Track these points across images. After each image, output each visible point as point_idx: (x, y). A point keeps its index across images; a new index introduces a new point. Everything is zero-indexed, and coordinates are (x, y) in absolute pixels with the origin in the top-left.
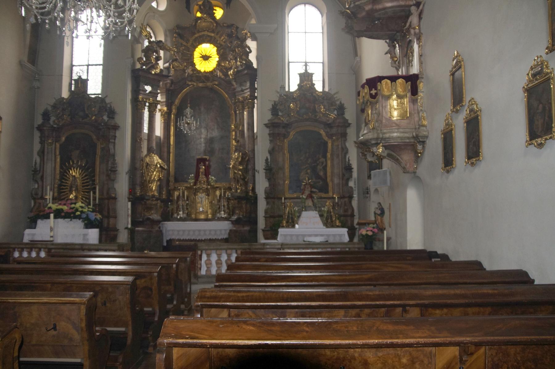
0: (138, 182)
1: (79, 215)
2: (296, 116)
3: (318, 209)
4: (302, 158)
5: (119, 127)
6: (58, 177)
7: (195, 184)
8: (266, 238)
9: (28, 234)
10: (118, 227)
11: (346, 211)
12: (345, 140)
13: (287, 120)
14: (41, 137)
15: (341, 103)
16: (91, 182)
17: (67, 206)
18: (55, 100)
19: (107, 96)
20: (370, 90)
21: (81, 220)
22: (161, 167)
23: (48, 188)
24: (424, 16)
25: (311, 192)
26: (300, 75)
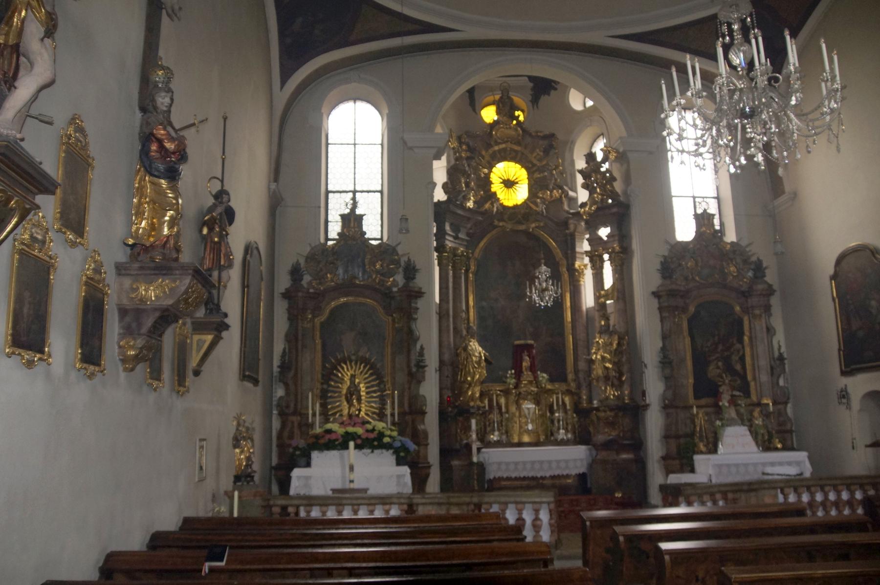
7: (517, 386)
9: (299, 478)
12: (770, 315)
14: (289, 310)
15: (758, 259)
18: (309, 249)
19: (399, 244)
21: (391, 451)
26: (343, 216)
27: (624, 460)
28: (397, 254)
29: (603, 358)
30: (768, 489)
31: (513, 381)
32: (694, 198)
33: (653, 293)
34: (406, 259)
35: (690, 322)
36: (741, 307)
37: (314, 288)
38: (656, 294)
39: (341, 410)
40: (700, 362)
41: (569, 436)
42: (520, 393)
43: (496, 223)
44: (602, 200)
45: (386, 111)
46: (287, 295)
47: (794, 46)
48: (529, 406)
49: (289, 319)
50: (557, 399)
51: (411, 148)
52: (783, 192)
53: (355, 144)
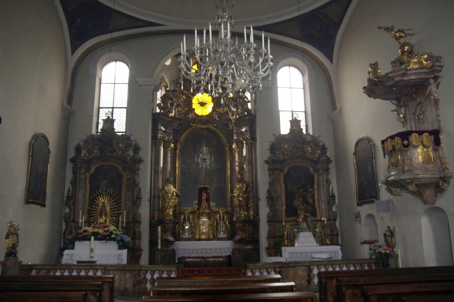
0: (156, 208)
1: (114, 238)
2: (289, 154)
3: (311, 230)
4: (295, 188)
5: (143, 160)
6: (87, 202)
7: (198, 209)
8: (270, 255)
9: (67, 255)
10: (142, 248)
11: (332, 231)
12: (328, 174)
14: (73, 168)
15: (323, 144)
16: (118, 208)
17: (102, 229)
18: (86, 137)
19: (132, 135)
20: (403, 141)
21: (116, 242)
22: (176, 195)
23: (81, 212)
24: (440, 86)
25: (305, 216)
27: (248, 249)
28: (131, 140)
29: (238, 195)
30: (301, 266)
31: (197, 206)
32: (292, 112)
35: (285, 176)
36: (313, 169)
37: (87, 157)
38: (266, 162)
39: (97, 220)
40: (290, 197)
43: (191, 124)
44: (242, 112)
45: (130, 67)
46: (73, 160)
47: (198, 40)
49: (73, 173)
50: (220, 216)
51: (140, 86)
52: (336, 109)
53: (115, 84)
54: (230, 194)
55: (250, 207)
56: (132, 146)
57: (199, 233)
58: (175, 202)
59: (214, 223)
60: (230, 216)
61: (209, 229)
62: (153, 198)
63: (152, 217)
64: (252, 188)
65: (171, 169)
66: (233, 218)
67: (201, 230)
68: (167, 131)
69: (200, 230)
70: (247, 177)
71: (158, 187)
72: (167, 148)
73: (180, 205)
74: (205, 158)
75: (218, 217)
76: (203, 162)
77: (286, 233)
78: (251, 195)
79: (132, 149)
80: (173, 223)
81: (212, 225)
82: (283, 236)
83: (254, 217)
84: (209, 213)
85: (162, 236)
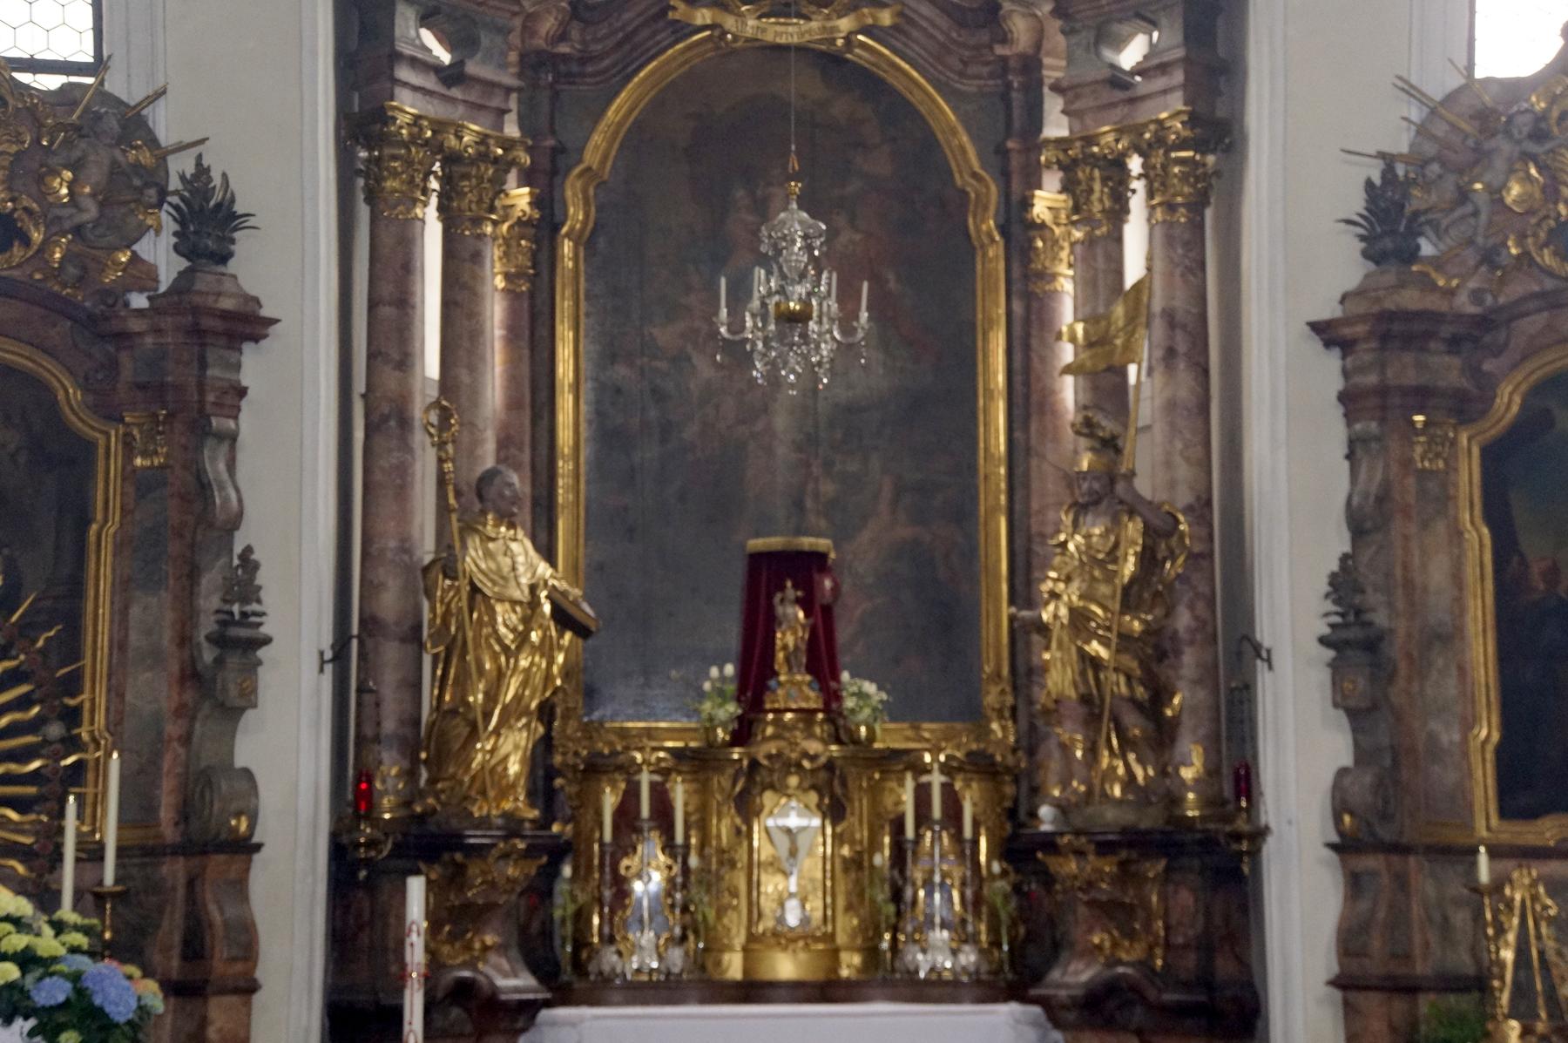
0: (389, 725)
2: (1547, 258)
7: (743, 733)
13: (1476, 296)
16: (55, 730)
19: (162, 93)
28: (152, 142)
29: (1079, 619)
31: (732, 708)
33: (1318, 328)
34: (190, 170)
35: (1495, 457)
38: (1325, 332)
41: (969, 957)
42: (754, 764)
48: (792, 817)
50: (922, 793)
54: (1006, 610)
55: (1175, 722)
56: (163, 193)
57: (752, 938)
58: (548, 677)
59: (874, 845)
60: (1009, 790)
61: (830, 893)
62: (354, 645)
63: (352, 794)
64: (1201, 559)
65: (513, 404)
66: (1033, 815)
67: (767, 905)
68: (472, 68)
69: (754, 912)
70: (1152, 466)
71: (406, 547)
72: (477, 221)
73: (590, 694)
74: (796, 305)
75: (908, 797)
76: (781, 337)
77: (1508, 955)
78: (1183, 620)
79: (169, 225)
80: (529, 854)
81: (856, 864)
82: (1479, 983)
83: (1212, 802)
84: (830, 766)
85: (435, 962)
